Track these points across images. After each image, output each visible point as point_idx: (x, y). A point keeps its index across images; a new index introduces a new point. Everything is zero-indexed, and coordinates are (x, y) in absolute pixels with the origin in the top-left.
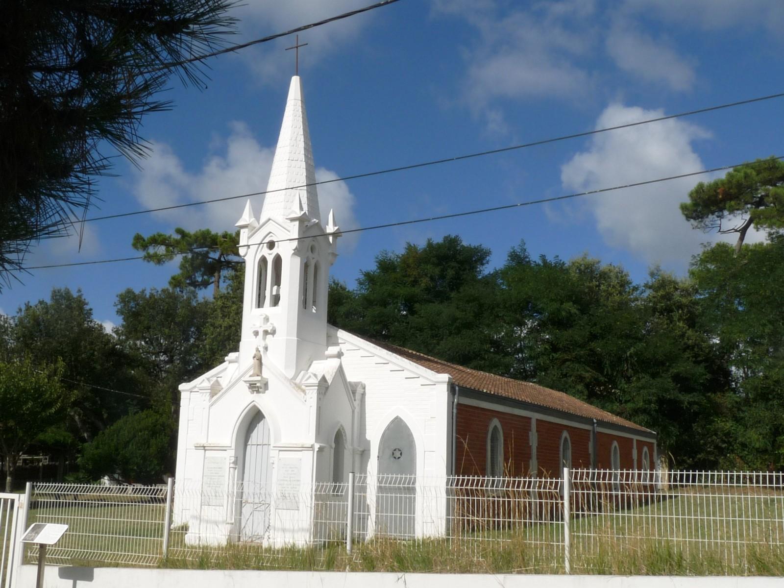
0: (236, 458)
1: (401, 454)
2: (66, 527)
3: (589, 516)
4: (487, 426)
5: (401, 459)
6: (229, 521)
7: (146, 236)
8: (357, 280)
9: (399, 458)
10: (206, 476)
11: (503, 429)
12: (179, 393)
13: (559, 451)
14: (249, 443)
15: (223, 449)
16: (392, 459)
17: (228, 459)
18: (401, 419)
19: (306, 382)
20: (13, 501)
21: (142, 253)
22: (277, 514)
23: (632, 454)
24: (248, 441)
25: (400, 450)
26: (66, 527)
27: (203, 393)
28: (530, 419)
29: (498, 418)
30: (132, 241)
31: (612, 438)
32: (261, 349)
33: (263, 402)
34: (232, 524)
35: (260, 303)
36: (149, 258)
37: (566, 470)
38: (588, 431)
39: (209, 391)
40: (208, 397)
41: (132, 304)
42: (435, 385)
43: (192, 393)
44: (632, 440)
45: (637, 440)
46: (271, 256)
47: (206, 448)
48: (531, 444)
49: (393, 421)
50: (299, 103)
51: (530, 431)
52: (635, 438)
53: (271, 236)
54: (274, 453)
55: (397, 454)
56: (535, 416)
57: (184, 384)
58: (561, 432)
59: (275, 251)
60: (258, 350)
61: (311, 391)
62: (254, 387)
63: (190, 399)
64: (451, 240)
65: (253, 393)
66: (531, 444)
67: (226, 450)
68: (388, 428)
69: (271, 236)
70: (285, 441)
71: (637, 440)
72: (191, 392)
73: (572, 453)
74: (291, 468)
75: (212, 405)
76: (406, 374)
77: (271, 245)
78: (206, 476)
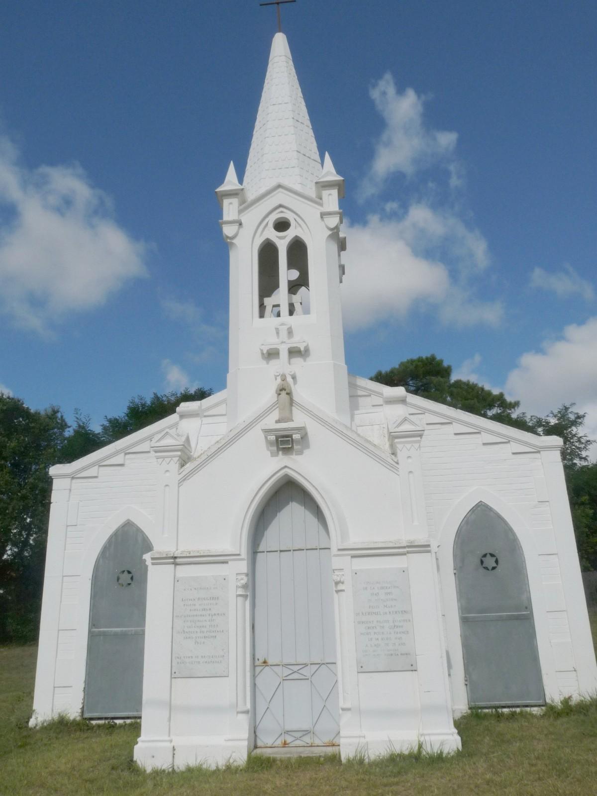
1: (497, 562)
5: (133, 585)
6: (241, 708)
8: (102, 426)
9: (494, 568)
10: (177, 616)
14: (261, 548)
15: (221, 559)
16: (482, 570)
18: (487, 506)
19: (397, 430)
22: (287, 678)
24: (259, 545)
25: (492, 555)
27: (164, 458)
33: (305, 468)
34: (247, 712)
39: (179, 453)
40: (174, 465)
42: (539, 452)
43: (74, 481)
46: (282, 241)
47: (178, 560)
49: (473, 510)
50: (291, 63)
53: (282, 212)
55: (490, 562)
57: (58, 466)
59: (290, 234)
61: (408, 446)
62: (285, 443)
63: (70, 490)
64: (202, 392)
65: (277, 455)
67: (226, 562)
68: (466, 521)
69: (282, 212)
70: (355, 539)
72: (73, 478)
74: (382, 588)
75: (185, 479)
78: (177, 616)
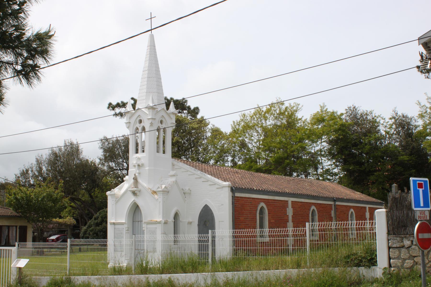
0: (128, 228)
2: (28, 260)
3: (240, 249)
4: (257, 207)
7: (114, 103)
11: (267, 208)
12: (106, 198)
13: (309, 217)
15: (122, 224)
17: (125, 228)
20: (11, 250)
21: (113, 112)
23: (365, 216)
26: (28, 260)
28: (287, 201)
29: (264, 202)
30: (107, 105)
31: (351, 207)
32: (137, 175)
35: (137, 152)
36: (116, 115)
37: (69, 240)
38: (332, 205)
41: (107, 143)
44: (365, 208)
45: (369, 207)
48: (288, 214)
49: (204, 207)
51: (288, 207)
52: (367, 206)
54: (144, 225)
56: (290, 200)
58: (310, 207)
59: (142, 124)
60: (135, 175)
62: (134, 193)
66: (288, 214)
71: (369, 207)
73: (318, 217)
76: (210, 183)
77: (140, 121)
